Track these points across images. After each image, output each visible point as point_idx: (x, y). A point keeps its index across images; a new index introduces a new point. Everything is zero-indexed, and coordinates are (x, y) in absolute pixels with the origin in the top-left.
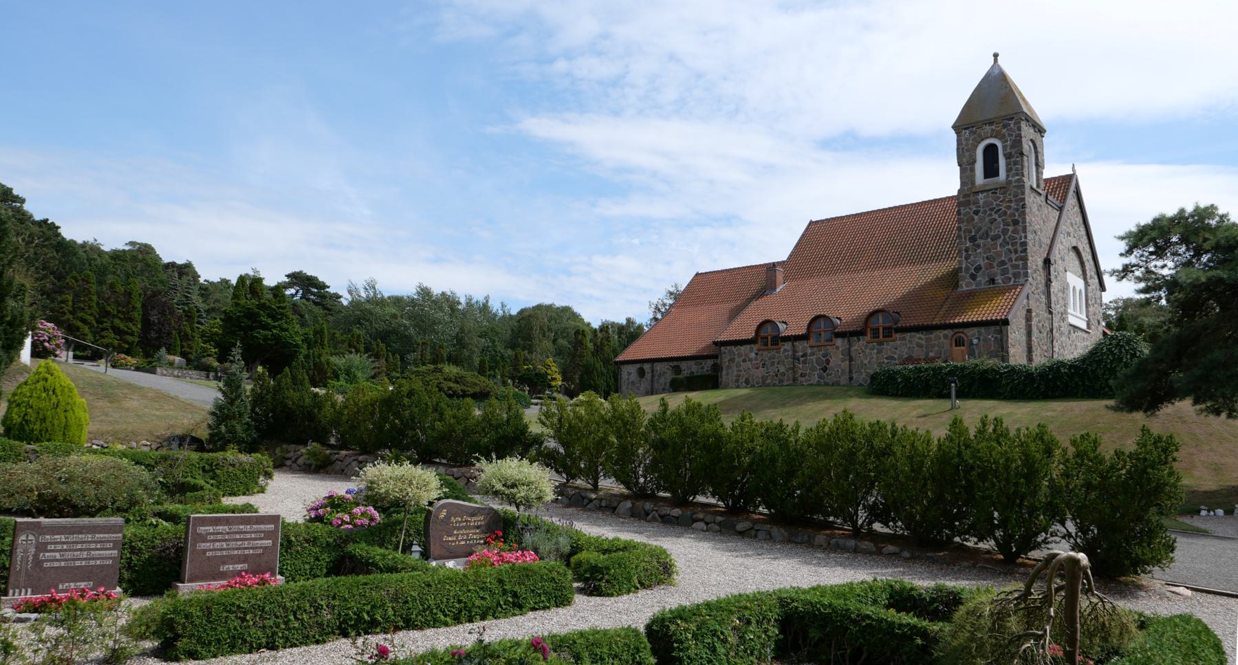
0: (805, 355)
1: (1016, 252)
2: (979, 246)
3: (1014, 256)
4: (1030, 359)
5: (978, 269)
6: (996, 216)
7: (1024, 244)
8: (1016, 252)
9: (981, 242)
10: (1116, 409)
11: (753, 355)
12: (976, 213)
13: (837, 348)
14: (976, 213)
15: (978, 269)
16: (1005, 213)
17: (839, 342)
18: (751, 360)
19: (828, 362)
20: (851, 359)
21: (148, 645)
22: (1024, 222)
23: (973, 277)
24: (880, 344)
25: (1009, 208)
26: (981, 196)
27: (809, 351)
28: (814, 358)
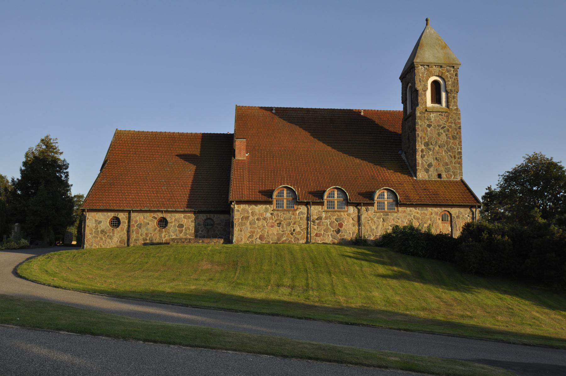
0: (320, 218)
1: (455, 157)
2: (430, 149)
3: (454, 161)
4: (239, 202)
5: (430, 165)
6: (442, 131)
7: (460, 153)
8: (455, 157)
9: (431, 146)
10: (21, 170)
11: (268, 215)
12: (429, 126)
13: (349, 215)
14: (429, 126)
15: (430, 165)
16: (448, 130)
17: (351, 209)
18: (265, 219)
19: (341, 225)
20: (359, 225)
21: (75, 199)
22: (460, 138)
23: (427, 171)
24: (386, 214)
25: (450, 127)
26: (432, 115)
27: (324, 215)
28: (328, 221)
